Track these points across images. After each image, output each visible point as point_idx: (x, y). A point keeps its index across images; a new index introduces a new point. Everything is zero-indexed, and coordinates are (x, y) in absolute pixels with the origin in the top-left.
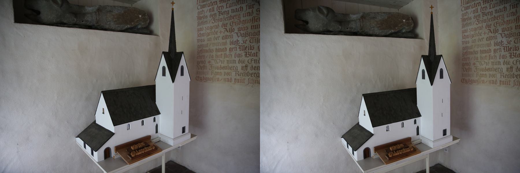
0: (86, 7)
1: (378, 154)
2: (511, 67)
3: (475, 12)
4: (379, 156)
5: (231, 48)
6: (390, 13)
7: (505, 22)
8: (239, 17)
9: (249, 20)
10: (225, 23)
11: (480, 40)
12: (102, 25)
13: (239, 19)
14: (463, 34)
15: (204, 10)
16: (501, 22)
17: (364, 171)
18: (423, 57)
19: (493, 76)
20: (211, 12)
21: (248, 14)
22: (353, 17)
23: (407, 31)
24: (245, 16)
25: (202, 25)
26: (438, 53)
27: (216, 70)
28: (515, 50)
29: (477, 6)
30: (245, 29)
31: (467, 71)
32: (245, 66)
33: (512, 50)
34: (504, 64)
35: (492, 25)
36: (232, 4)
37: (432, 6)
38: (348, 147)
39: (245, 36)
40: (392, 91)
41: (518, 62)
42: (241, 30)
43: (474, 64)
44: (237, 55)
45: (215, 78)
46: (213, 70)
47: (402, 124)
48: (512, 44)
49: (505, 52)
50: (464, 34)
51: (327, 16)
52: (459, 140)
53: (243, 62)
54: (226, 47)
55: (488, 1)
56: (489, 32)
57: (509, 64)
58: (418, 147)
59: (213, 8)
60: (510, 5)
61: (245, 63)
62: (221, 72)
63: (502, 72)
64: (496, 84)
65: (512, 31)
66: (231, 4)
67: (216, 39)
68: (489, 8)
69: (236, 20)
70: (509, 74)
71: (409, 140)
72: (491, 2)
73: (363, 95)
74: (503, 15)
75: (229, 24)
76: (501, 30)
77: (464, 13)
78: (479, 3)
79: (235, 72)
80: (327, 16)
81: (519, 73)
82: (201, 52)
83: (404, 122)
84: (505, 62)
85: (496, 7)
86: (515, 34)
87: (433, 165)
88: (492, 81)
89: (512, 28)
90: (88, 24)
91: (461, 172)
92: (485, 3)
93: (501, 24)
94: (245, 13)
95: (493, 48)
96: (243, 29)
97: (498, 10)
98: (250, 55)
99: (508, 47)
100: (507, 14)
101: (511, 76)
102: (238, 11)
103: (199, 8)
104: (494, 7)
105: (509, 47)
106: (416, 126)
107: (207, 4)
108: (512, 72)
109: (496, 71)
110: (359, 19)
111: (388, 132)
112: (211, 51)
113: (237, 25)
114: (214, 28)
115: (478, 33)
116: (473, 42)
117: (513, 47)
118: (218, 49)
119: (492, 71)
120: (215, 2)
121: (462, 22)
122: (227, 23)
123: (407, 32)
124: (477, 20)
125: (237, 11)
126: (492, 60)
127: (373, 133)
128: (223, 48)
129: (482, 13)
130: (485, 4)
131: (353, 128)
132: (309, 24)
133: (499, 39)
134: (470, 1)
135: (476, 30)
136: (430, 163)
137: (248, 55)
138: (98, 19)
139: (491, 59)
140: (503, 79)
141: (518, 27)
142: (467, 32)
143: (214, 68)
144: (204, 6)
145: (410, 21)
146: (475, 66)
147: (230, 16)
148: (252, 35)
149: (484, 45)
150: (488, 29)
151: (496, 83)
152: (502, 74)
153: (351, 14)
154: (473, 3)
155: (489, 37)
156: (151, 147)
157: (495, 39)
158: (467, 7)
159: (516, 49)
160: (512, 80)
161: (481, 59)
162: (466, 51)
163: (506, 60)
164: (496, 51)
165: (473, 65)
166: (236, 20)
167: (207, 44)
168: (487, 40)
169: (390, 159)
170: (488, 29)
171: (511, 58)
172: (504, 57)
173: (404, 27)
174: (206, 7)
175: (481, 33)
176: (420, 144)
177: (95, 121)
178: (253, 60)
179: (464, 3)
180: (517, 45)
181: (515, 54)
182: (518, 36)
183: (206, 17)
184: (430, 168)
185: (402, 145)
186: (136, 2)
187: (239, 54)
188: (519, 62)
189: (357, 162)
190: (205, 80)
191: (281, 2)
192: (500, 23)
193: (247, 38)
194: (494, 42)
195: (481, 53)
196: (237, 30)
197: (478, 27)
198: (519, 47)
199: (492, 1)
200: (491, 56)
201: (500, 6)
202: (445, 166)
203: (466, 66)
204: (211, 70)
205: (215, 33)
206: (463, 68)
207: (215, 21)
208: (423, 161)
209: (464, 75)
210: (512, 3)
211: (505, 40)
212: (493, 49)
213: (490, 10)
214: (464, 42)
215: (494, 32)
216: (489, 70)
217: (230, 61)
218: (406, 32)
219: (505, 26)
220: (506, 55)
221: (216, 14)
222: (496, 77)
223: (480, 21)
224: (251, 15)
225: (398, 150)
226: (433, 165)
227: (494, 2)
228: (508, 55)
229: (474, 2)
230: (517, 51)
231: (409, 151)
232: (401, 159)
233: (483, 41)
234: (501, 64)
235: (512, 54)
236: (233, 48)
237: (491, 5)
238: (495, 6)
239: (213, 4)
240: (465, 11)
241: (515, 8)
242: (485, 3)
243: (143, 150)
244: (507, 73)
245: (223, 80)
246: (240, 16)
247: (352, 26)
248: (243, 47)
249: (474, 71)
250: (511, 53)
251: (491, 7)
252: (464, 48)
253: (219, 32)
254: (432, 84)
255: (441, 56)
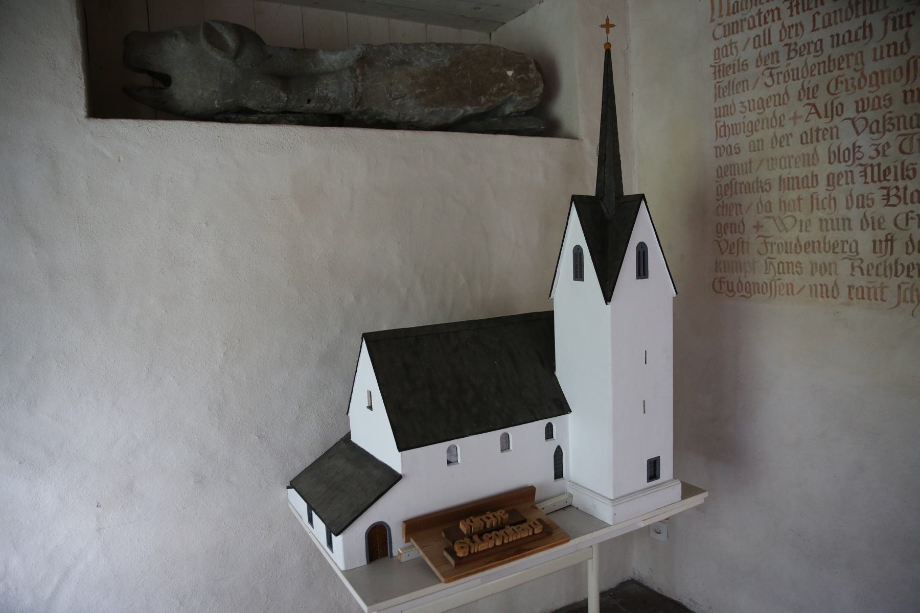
0: (321, 52)
1: (418, 545)
2: (889, 237)
3: (762, 44)
4: (421, 553)
5: (833, 174)
6: (458, 46)
7: (865, 79)
8: (859, 61)
9: (895, 72)
10: (811, 86)
11: (778, 142)
12: (375, 108)
13: (860, 67)
14: (717, 121)
15: (736, 43)
16: (852, 78)
17: (368, 604)
18: (578, 201)
19: (825, 269)
20: (760, 46)
21: (892, 47)
22: (331, 59)
23: (521, 112)
24: (882, 58)
25: (729, 95)
26: (630, 188)
27: (784, 254)
28: (903, 179)
29: (768, 20)
30: (882, 103)
31: (731, 253)
32: (883, 239)
33: (891, 177)
34: (865, 227)
35: (823, 87)
36: (833, 15)
37: (608, 20)
38: (311, 521)
39: (881, 129)
40: (469, 323)
41: (912, 218)
42: (866, 108)
43: (758, 227)
44: (855, 199)
45: (778, 283)
46: (772, 256)
47: (502, 438)
48: (893, 157)
49: (866, 183)
50: (723, 119)
51: (238, 53)
52: (705, 495)
53: (877, 224)
54: (816, 170)
55: (808, 5)
56: (810, 113)
57: (880, 228)
58: (557, 520)
59: (767, 32)
60: (886, 19)
61: (884, 229)
62: (798, 262)
63: (858, 253)
64: (835, 298)
65: (891, 109)
66: (829, 14)
67: (781, 143)
68: (809, 27)
69: (848, 73)
70: (881, 264)
71: (526, 494)
72: (816, 7)
73: (367, 337)
74: (861, 52)
75: (825, 87)
76: (854, 106)
77: (721, 46)
78: (776, 12)
79: (849, 263)
80: (238, 53)
81: (916, 258)
82: (729, 193)
83: (510, 431)
84: (867, 220)
85: (836, 23)
86: (902, 120)
87: (613, 587)
88: (821, 285)
89: (890, 99)
90: (327, 108)
91: (710, 608)
92: (795, 9)
93: (853, 86)
94: (882, 47)
95: (823, 169)
96: (873, 106)
97: (844, 36)
98: (902, 199)
99: (879, 165)
100: (875, 49)
101: (888, 269)
102: (857, 40)
103: (717, 36)
104: (827, 24)
105: (883, 168)
106: (552, 446)
107: (745, 19)
108: (891, 254)
109: (836, 250)
110: (352, 69)
111: (453, 467)
112: (763, 186)
113: (852, 90)
114: (771, 104)
115: (770, 116)
116: (754, 150)
117: (896, 167)
118: (788, 178)
119: (820, 252)
120: (772, 11)
121: (715, 79)
122: (817, 86)
123: (520, 114)
124: (767, 72)
125: (850, 41)
126: (821, 214)
127: (399, 470)
128: (806, 176)
129: (786, 45)
130: (798, 13)
131: (329, 454)
132: (172, 86)
133: (847, 139)
134: (744, 2)
135: (763, 107)
136: (601, 577)
137: (895, 198)
138: (360, 90)
139: (818, 209)
140: (861, 281)
141: (913, 96)
142: (732, 114)
143: (775, 247)
144: (735, 25)
145: (532, 76)
146: (761, 233)
147: (826, 60)
148: (908, 126)
149: (793, 161)
150: (805, 101)
151: (836, 295)
152: (856, 264)
153: (321, 52)
154: (754, 11)
155: (809, 132)
156: (530, 526)
157: (832, 138)
158: (733, 23)
159: (907, 173)
160: (893, 282)
161: (783, 208)
162: (729, 182)
163: (869, 212)
164: (836, 180)
165: (754, 230)
166: (848, 73)
167: (750, 162)
168: (804, 141)
169: (460, 562)
170: (808, 104)
171: (886, 205)
172: (863, 202)
173: (511, 97)
174: (742, 31)
175: (783, 115)
176: (568, 510)
177: (349, 435)
178: (914, 215)
179: (721, 11)
180: (909, 160)
181: (902, 190)
182: (912, 127)
183: (745, 66)
184: (602, 595)
185: (501, 514)
186: (504, 23)
187: (863, 196)
188: (917, 220)
189: (345, 573)
190: (744, 293)
191: (74, 9)
192: (850, 82)
193: (888, 137)
194: (829, 149)
195: (780, 190)
196: (855, 111)
197: (770, 97)
198: (916, 167)
199: (822, 4)
200: (817, 199)
201: (849, 20)
202: (656, 590)
203: (729, 233)
204: (765, 257)
205: (774, 124)
206: (719, 243)
207: (773, 82)
208: (577, 572)
209: (722, 266)
210: (892, 12)
211: (865, 141)
212: (825, 175)
213: (815, 36)
214: (722, 148)
215: (829, 114)
216: (810, 247)
217: (832, 221)
218: (517, 112)
219: (866, 92)
220: (870, 197)
221: (777, 52)
222: (836, 274)
223: (778, 73)
224: (902, 53)
225: (490, 532)
226: (613, 583)
227: (829, 7)
228: (878, 195)
229: (759, 6)
230: (908, 182)
231: (529, 536)
232: (501, 564)
233: (788, 145)
234: (852, 227)
235: (893, 192)
236: (841, 173)
237: (819, 19)
238: (832, 21)
239: (765, 18)
240: (726, 41)
241: (901, 27)
242: (795, 9)
243: (497, 535)
244: (875, 259)
245: (807, 291)
246: (862, 56)
247: (325, 91)
248: (876, 169)
249: (758, 252)
250: (888, 189)
251: (819, 24)
252: (721, 172)
253: (790, 119)
254: (608, 299)
255: (642, 197)
